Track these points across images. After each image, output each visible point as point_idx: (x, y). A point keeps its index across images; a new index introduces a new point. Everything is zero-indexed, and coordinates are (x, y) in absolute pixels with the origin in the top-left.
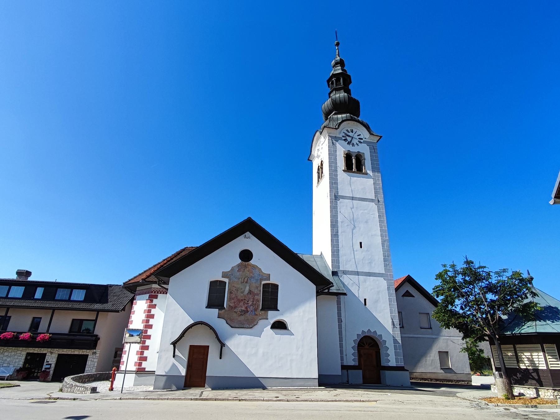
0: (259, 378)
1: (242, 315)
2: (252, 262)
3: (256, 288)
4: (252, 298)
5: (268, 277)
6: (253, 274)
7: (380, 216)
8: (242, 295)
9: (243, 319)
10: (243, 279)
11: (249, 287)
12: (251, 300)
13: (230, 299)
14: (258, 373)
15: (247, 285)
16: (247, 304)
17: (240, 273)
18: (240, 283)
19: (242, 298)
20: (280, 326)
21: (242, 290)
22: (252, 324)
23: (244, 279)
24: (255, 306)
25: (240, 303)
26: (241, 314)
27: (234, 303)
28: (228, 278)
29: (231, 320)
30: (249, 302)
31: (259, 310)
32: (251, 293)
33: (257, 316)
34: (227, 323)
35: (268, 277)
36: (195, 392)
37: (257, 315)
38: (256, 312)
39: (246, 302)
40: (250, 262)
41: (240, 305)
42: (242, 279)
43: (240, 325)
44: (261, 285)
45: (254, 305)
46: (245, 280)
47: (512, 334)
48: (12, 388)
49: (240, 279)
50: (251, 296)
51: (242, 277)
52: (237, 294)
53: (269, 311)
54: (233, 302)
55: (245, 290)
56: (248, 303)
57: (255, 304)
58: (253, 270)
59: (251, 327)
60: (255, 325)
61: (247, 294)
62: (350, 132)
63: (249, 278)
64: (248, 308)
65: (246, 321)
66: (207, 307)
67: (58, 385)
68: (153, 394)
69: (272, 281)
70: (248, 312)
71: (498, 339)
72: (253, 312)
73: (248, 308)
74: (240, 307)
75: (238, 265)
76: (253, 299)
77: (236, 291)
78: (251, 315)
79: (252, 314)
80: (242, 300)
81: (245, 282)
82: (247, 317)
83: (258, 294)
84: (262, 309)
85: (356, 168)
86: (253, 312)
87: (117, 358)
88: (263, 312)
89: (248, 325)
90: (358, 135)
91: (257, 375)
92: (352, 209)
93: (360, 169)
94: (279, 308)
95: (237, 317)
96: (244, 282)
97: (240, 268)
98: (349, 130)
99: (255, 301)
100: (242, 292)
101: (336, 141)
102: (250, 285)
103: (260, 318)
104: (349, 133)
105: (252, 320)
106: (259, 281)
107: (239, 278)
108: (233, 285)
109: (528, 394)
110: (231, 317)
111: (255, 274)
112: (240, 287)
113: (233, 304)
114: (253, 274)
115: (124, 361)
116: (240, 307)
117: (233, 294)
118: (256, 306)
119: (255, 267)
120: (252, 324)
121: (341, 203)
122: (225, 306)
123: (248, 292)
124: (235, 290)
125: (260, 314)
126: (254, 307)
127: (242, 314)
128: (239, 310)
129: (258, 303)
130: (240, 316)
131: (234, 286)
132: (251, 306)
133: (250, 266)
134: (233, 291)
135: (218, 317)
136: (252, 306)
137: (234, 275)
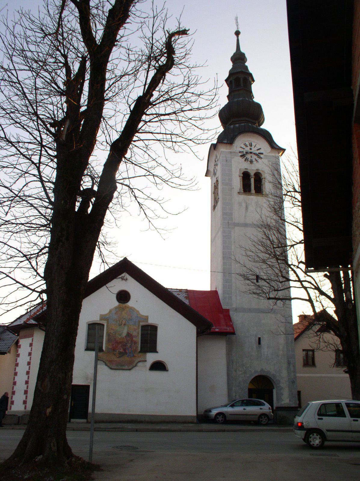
2: (130, 304)
5: (147, 318)
13: (109, 340)
20: (159, 366)
35: (147, 318)
47: (344, 283)
49: (118, 322)
59: (130, 368)
62: (248, 145)
67: (289, 209)
69: (151, 321)
71: (352, 300)
75: (116, 308)
83: (136, 337)
84: (141, 352)
85: (255, 189)
87: (9, 396)
88: (141, 354)
90: (257, 149)
93: (259, 190)
94: (157, 350)
96: (121, 325)
98: (247, 143)
100: (120, 335)
104: (247, 147)
107: (117, 321)
109: (35, 45)
115: (88, 349)
119: (132, 309)
122: (104, 348)
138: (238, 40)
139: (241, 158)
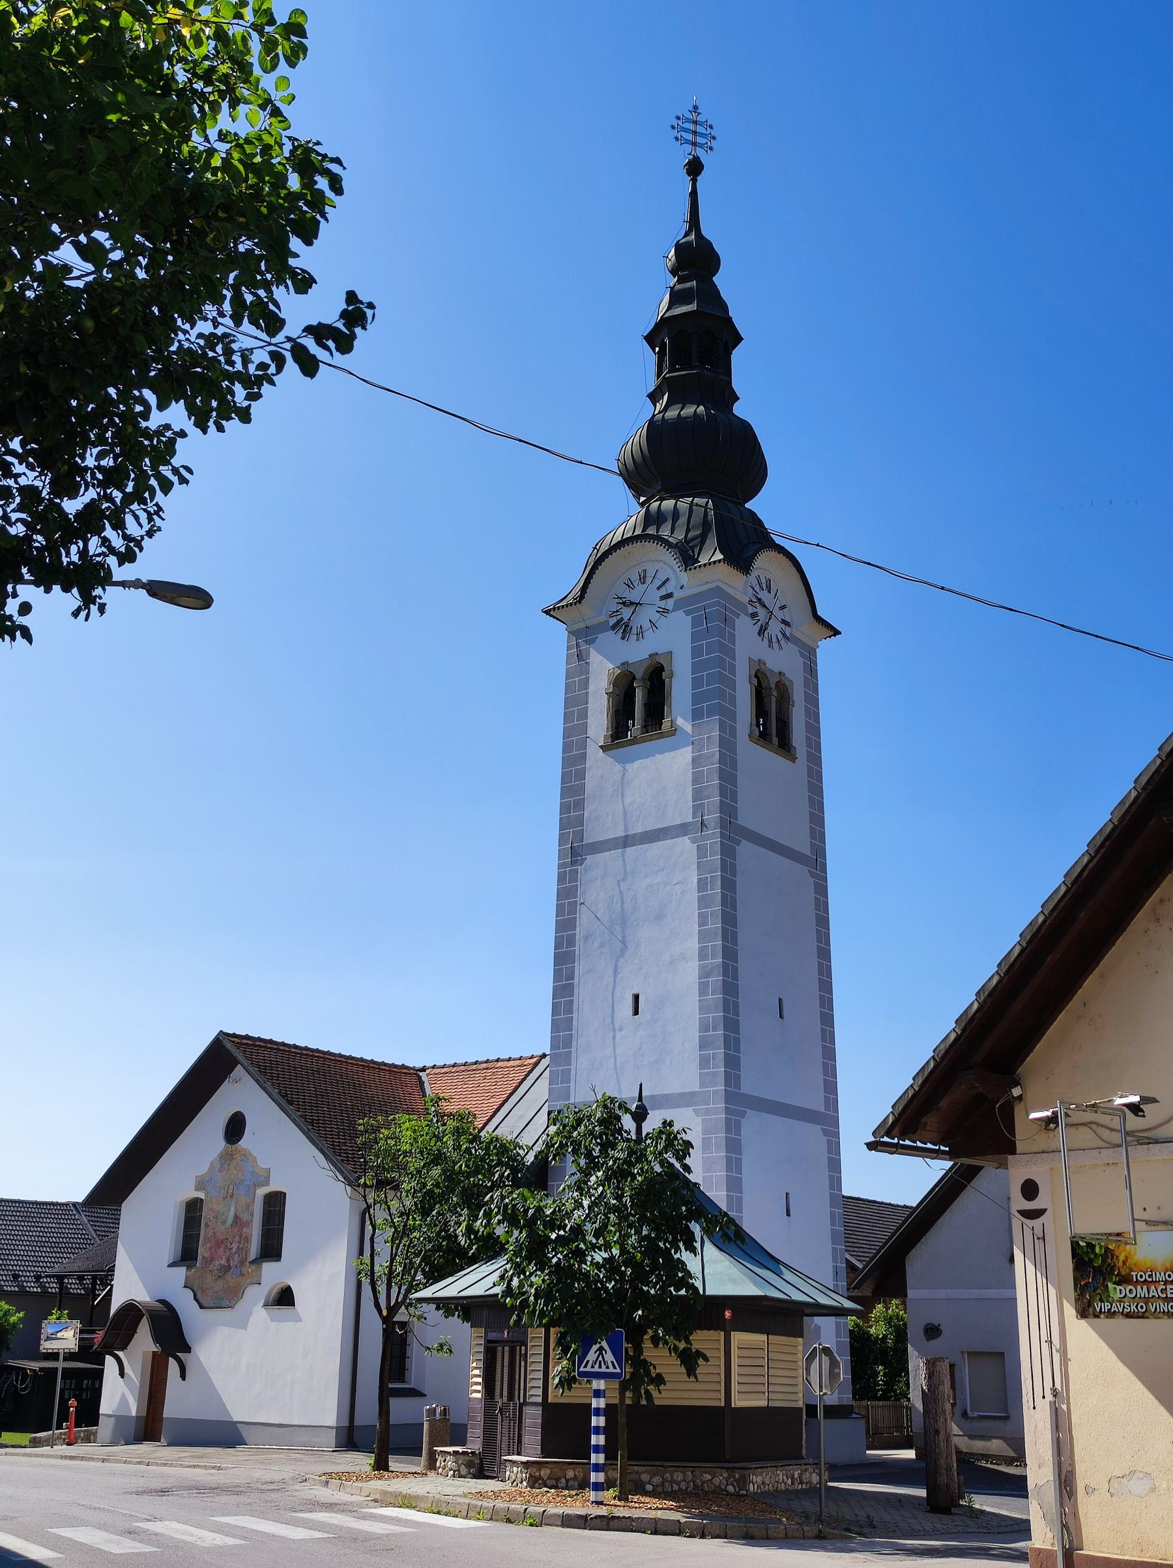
0: (961, 1433)
6: (243, 1174)
7: (702, 885)
12: (237, 1239)
14: (238, 1413)
28: (204, 1189)
36: (145, 1448)
37: (244, 1275)
39: (229, 1244)
53: (264, 1264)
57: (242, 1249)
61: (231, 1225)
68: (321, 1459)
76: (240, 1236)
80: (222, 1242)
86: (239, 1269)
88: (253, 1267)
91: (236, 1417)
92: (621, 884)
100: (224, 1222)
101: (587, 642)
103: (248, 1281)
121: (598, 866)
122: (1049, 1113)
130: (217, 1280)
138: (694, 194)
139: (612, 633)
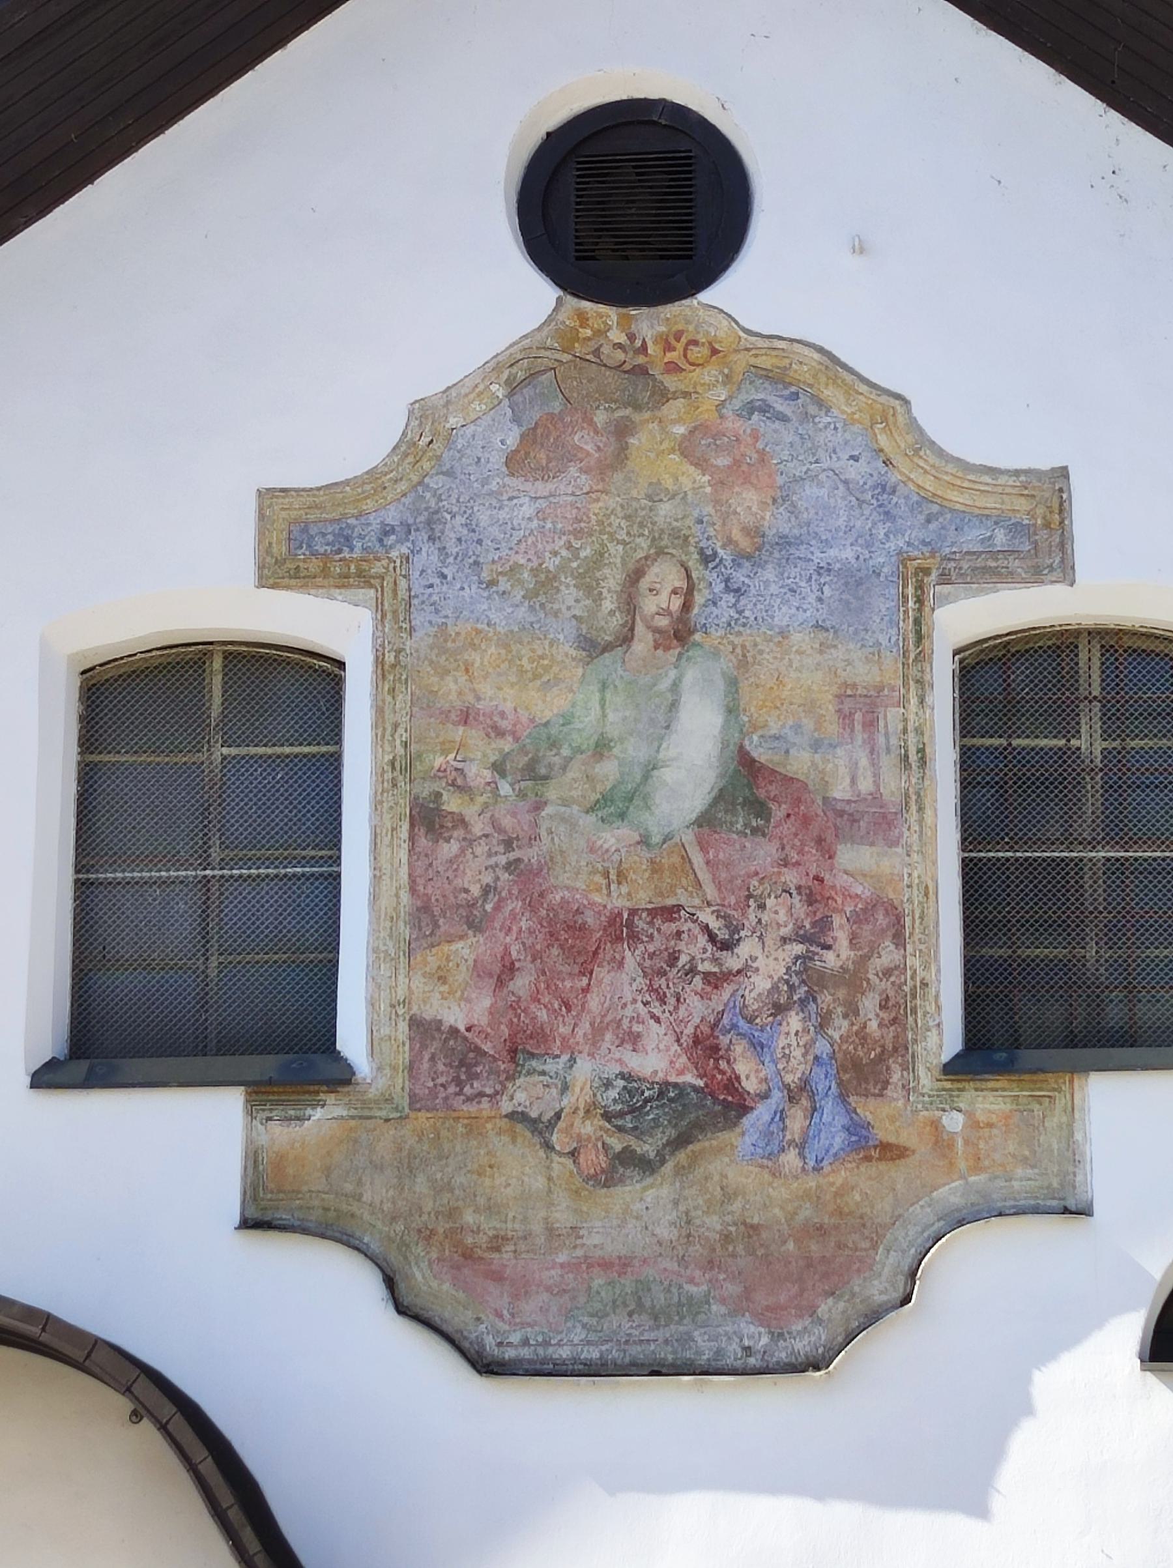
1: (647, 1166)
3: (846, 718)
4: (791, 877)
6: (782, 498)
8: (614, 838)
9: (665, 1232)
10: (612, 579)
11: (732, 711)
15: (691, 675)
16: (715, 981)
17: (560, 486)
18: (567, 649)
19: (619, 901)
21: (608, 770)
22: (825, 1308)
23: (636, 575)
24: (852, 1011)
25: (602, 973)
26: (617, 1143)
27: (500, 983)
29: (468, 1255)
30: (747, 948)
31: (926, 1080)
32: (759, 808)
33: (898, 1174)
34: (402, 1309)
37: (891, 1152)
38: (867, 1109)
39: (695, 949)
40: (706, 296)
41: (594, 1002)
42: (590, 588)
43: (619, 1322)
44: (923, 657)
45: (825, 999)
46: (650, 605)
48: (618, 1382)
49: (569, 595)
50: (764, 853)
51: (600, 556)
52: (534, 838)
54: (479, 970)
55: (650, 768)
56: (732, 962)
58: (768, 428)
59: (802, 1346)
60: (873, 1317)
61: (705, 821)
63: (707, 558)
64: (739, 1048)
65: (711, 1264)
66: (51, 1065)
70: (744, 1110)
72: (829, 1108)
73: (739, 1048)
74: (598, 1032)
77: (505, 788)
78: (791, 1158)
79: (815, 1148)
81: (642, 643)
82: (729, 1195)
89: (760, 1318)
95: (563, 1200)
96: (626, 638)
97: (556, 406)
99: (840, 934)
102: (733, 684)
103: (951, 1193)
105: (821, 1231)
106: (882, 602)
108: (452, 689)
110: (452, 1213)
111: (810, 490)
112: (567, 720)
113: (484, 1001)
114: (782, 498)
116: (598, 1032)
117: (469, 842)
118: (869, 1004)
120: (825, 1308)
123: (722, 798)
124: (498, 768)
125: (941, 1142)
126: (840, 1027)
127: (647, 1148)
128: (578, 1096)
129: (888, 955)
131: (466, 717)
132: (779, 1009)
133: (709, 374)
134: (462, 788)
135: (249, 1224)
136: (794, 1021)
137: (454, 528)
